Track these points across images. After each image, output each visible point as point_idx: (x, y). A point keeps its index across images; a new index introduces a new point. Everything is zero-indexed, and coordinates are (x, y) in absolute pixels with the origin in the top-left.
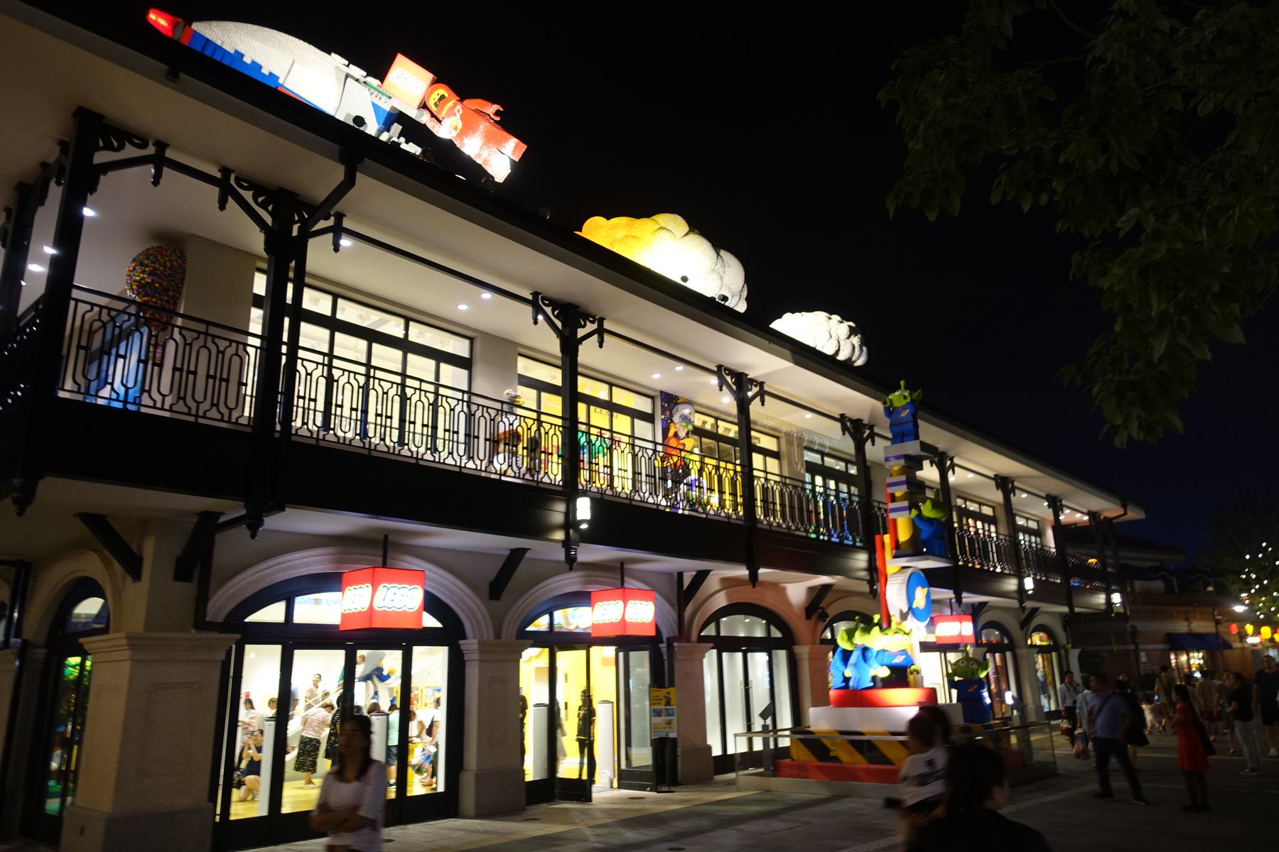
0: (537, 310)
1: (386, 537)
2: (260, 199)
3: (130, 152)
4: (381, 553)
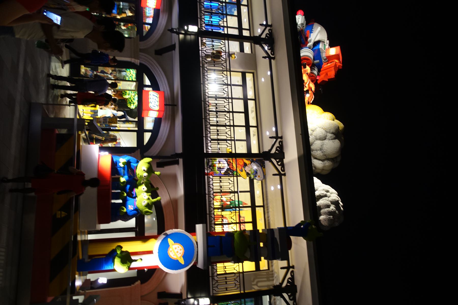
0: (277, 137)
1: (176, 105)
2: (290, 280)
3: (279, 168)
4: (170, 104)
